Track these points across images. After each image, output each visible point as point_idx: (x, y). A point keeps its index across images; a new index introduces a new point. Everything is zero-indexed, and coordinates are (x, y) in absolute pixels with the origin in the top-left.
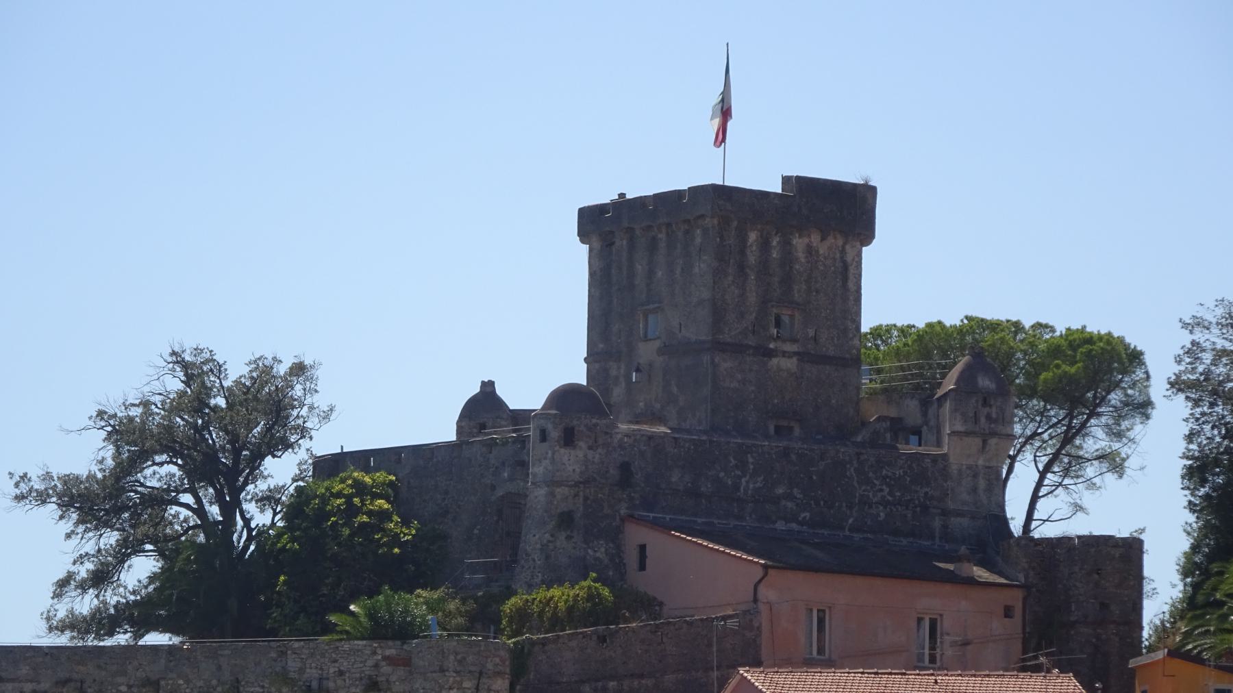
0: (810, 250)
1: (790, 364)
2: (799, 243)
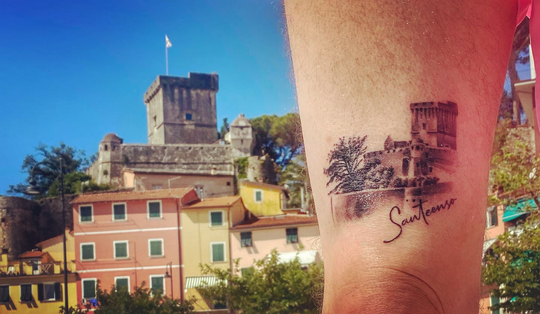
0: (197, 95)
1: (193, 127)
2: (193, 93)
